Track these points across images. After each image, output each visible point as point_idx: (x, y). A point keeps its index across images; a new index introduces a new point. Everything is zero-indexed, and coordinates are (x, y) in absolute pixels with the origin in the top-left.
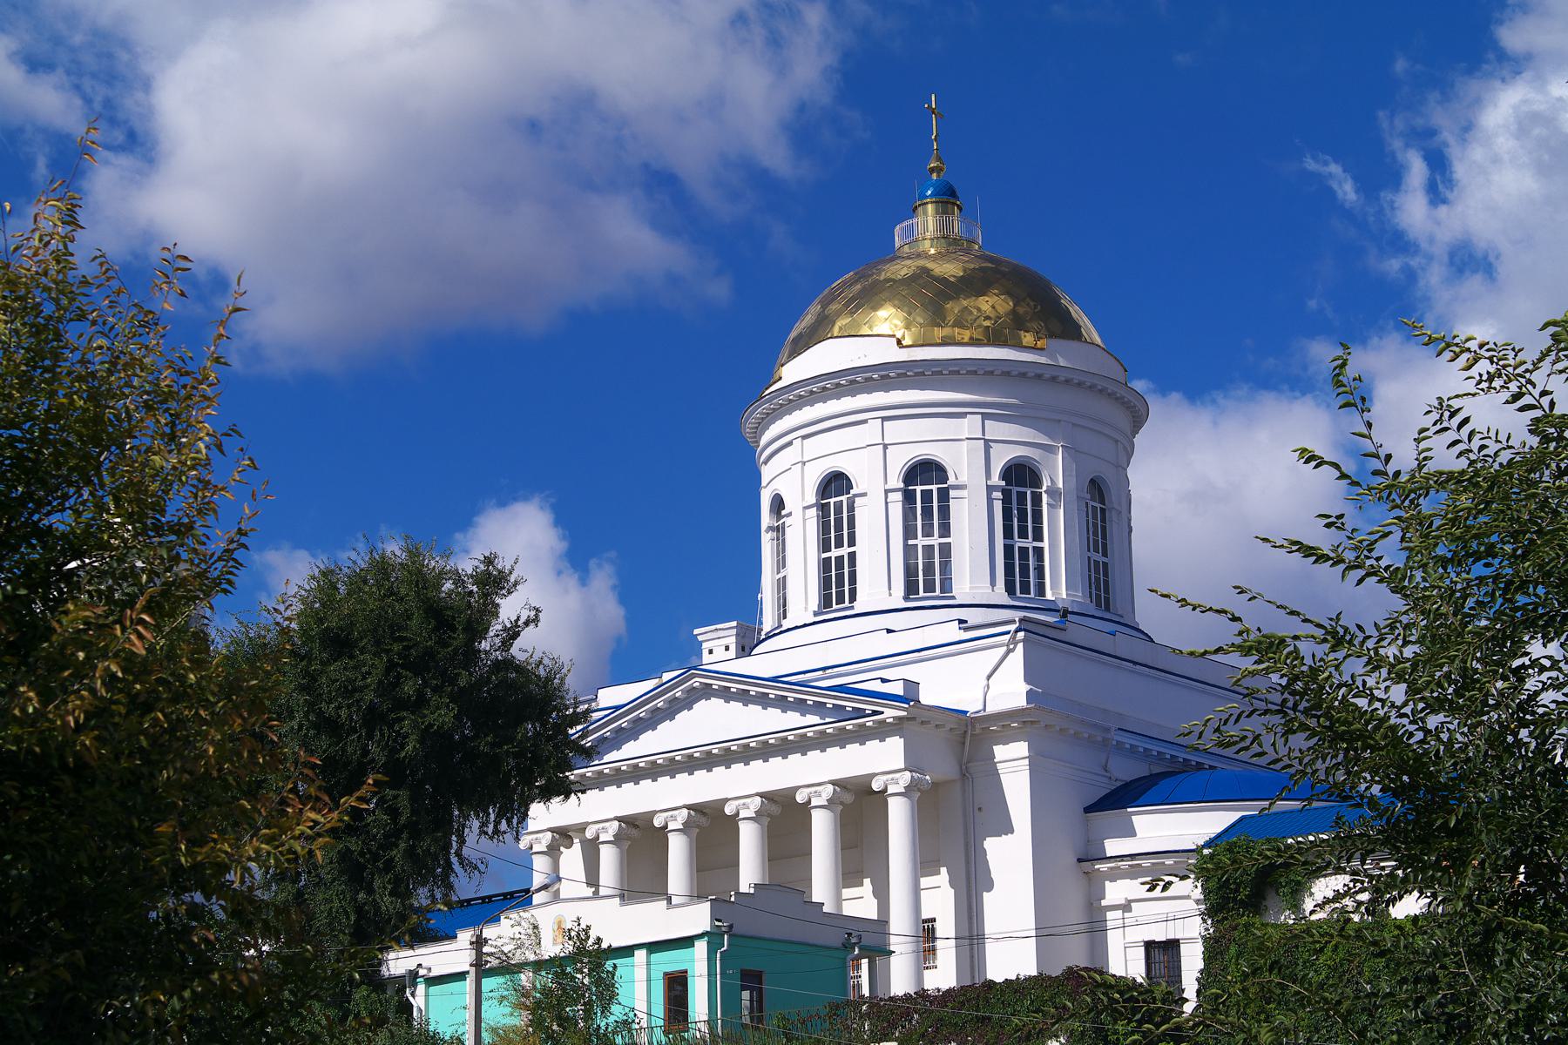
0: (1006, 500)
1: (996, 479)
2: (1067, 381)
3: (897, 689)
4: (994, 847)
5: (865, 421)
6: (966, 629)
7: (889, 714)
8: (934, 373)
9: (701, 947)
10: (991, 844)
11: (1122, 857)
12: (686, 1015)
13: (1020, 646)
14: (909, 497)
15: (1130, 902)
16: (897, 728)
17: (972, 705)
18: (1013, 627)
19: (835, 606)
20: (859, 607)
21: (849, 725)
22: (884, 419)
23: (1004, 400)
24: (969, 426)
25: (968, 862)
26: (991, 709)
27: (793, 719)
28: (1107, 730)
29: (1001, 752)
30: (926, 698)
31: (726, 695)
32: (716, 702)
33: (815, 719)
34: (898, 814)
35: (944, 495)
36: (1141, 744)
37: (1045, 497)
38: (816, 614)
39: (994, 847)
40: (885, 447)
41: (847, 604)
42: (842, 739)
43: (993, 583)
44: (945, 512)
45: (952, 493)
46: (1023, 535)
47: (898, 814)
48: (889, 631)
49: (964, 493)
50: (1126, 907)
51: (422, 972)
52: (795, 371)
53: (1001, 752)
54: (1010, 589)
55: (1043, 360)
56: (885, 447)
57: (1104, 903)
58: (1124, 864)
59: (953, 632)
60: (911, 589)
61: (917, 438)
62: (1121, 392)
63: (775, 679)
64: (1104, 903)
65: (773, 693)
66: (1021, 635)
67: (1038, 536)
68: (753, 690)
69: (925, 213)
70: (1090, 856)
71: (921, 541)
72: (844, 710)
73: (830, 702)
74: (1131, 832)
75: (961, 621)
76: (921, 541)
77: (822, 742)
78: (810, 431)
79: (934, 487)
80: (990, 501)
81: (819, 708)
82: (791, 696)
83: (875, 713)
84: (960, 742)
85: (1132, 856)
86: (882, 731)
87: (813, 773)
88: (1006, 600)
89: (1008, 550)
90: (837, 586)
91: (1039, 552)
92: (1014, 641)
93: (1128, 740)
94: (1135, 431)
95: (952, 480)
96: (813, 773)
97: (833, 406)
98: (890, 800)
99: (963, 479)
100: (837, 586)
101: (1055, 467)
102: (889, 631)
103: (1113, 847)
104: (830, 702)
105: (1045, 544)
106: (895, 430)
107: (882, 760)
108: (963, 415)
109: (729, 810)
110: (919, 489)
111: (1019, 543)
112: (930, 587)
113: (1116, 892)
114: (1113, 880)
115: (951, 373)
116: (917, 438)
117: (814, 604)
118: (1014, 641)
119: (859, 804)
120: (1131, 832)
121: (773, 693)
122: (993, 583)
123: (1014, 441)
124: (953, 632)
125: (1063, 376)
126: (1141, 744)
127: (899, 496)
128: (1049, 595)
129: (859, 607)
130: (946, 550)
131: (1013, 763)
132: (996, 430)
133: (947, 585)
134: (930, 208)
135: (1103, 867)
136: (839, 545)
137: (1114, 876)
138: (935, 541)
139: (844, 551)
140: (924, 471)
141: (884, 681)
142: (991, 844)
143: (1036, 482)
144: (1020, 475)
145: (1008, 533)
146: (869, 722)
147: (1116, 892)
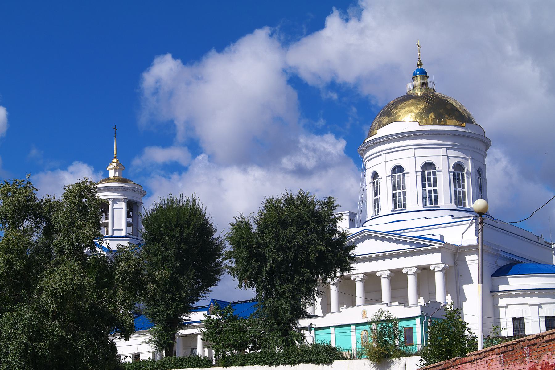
0: (454, 176)
1: (451, 169)
2: (464, 136)
3: (438, 238)
4: (466, 288)
5: (408, 149)
6: (454, 218)
7: (437, 246)
8: (432, 134)
9: (418, 320)
10: (465, 287)
11: (505, 291)
12: (413, 342)
13: (474, 224)
14: (423, 174)
15: (507, 305)
16: (438, 250)
17: (459, 244)
18: (472, 218)
19: (398, 209)
20: (408, 209)
21: (422, 249)
22: (415, 149)
23: (449, 143)
24: (443, 151)
25: (457, 292)
26: (465, 244)
27: (401, 246)
28: (498, 251)
29: (468, 258)
30: (446, 240)
31: (376, 238)
32: (372, 241)
33: (409, 247)
34: (439, 278)
35: (435, 174)
36: (506, 255)
37: (465, 175)
38: (392, 211)
39: (466, 288)
40: (415, 158)
41: (403, 208)
42: (419, 253)
43: (451, 202)
44: (435, 179)
45: (437, 173)
46: (459, 187)
47: (439, 278)
48: (426, 218)
49: (441, 173)
50: (506, 307)
51: (313, 326)
52: (381, 132)
53: (468, 258)
54: (456, 204)
55: (464, 130)
56: (415, 158)
57: (499, 305)
58: (506, 293)
59: (450, 219)
60: (425, 204)
61: (426, 155)
62: (481, 138)
63: (387, 232)
64: (499, 305)
65: (387, 237)
66: (474, 221)
67: (464, 187)
68: (380, 236)
69: (417, 79)
70: (494, 291)
71: (427, 188)
72: (422, 246)
73: (415, 242)
74: (507, 283)
75: (452, 216)
76: (427, 188)
77: (412, 254)
78: (388, 152)
79: (431, 171)
80: (450, 176)
81: (411, 243)
82: (394, 238)
83: (431, 245)
84: (455, 255)
85: (509, 291)
86: (434, 251)
87: (409, 264)
88: (455, 208)
89: (455, 191)
90: (399, 203)
91: (464, 192)
92: (472, 223)
93: (502, 254)
94: (487, 150)
95: (437, 169)
96: (409, 264)
97: (397, 144)
98: (436, 273)
99: (441, 169)
100: (399, 203)
101: (468, 165)
102: (426, 218)
103: (502, 288)
104: (415, 242)
105: (466, 190)
106: (419, 152)
107: (434, 260)
108: (441, 148)
109: (378, 274)
110: (426, 171)
111: (458, 189)
112: (431, 203)
113: (502, 302)
114: (502, 298)
115: (437, 134)
116: (426, 155)
117: (391, 207)
118: (472, 223)
119: (424, 273)
120: (507, 283)
121: (387, 237)
122: (451, 202)
123: (456, 156)
124: (450, 219)
125: (471, 136)
126: (506, 255)
127: (420, 174)
128: (467, 206)
129: (408, 209)
130: (435, 191)
131: (473, 263)
132: (452, 153)
133: (436, 203)
134: (419, 78)
135: (499, 294)
136: (399, 189)
137: (502, 297)
138: (432, 188)
139: (401, 191)
140: (429, 165)
141: (433, 235)
142: (465, 287)
143: (463, 170)
144: (459, 167)
145: (455, 186)
146: (430, 248)
147: (502, 302)
